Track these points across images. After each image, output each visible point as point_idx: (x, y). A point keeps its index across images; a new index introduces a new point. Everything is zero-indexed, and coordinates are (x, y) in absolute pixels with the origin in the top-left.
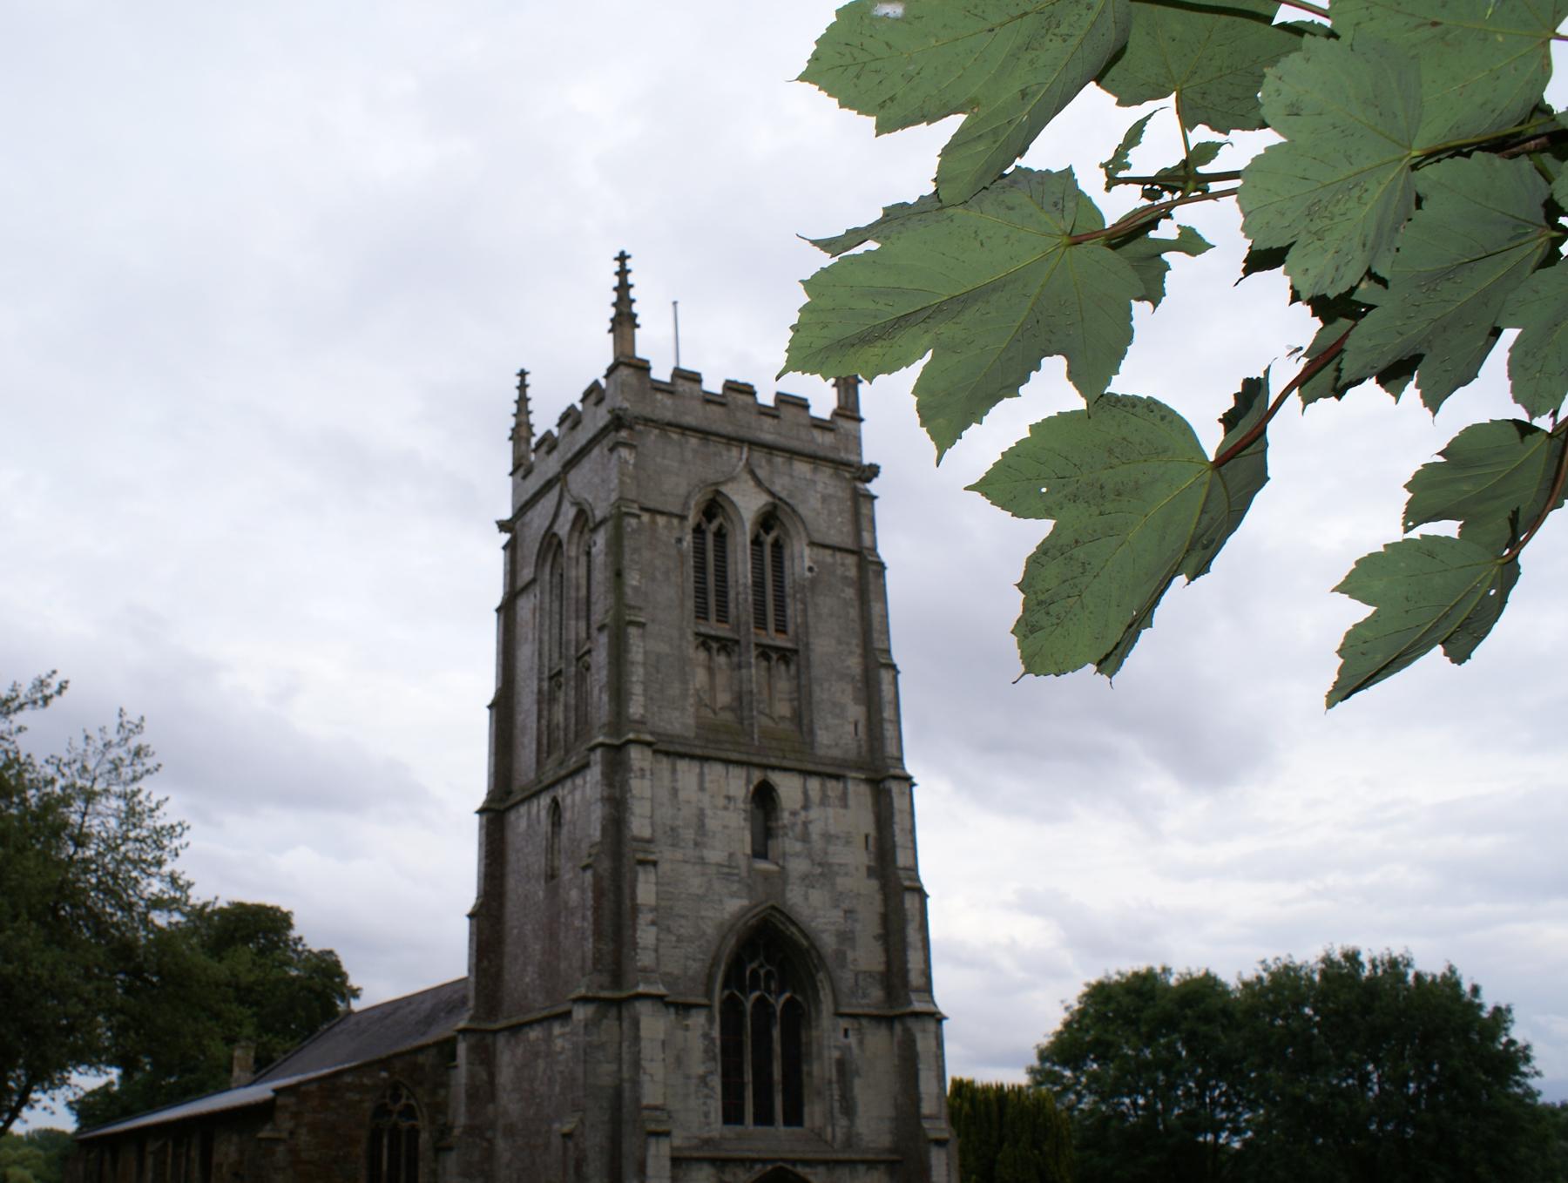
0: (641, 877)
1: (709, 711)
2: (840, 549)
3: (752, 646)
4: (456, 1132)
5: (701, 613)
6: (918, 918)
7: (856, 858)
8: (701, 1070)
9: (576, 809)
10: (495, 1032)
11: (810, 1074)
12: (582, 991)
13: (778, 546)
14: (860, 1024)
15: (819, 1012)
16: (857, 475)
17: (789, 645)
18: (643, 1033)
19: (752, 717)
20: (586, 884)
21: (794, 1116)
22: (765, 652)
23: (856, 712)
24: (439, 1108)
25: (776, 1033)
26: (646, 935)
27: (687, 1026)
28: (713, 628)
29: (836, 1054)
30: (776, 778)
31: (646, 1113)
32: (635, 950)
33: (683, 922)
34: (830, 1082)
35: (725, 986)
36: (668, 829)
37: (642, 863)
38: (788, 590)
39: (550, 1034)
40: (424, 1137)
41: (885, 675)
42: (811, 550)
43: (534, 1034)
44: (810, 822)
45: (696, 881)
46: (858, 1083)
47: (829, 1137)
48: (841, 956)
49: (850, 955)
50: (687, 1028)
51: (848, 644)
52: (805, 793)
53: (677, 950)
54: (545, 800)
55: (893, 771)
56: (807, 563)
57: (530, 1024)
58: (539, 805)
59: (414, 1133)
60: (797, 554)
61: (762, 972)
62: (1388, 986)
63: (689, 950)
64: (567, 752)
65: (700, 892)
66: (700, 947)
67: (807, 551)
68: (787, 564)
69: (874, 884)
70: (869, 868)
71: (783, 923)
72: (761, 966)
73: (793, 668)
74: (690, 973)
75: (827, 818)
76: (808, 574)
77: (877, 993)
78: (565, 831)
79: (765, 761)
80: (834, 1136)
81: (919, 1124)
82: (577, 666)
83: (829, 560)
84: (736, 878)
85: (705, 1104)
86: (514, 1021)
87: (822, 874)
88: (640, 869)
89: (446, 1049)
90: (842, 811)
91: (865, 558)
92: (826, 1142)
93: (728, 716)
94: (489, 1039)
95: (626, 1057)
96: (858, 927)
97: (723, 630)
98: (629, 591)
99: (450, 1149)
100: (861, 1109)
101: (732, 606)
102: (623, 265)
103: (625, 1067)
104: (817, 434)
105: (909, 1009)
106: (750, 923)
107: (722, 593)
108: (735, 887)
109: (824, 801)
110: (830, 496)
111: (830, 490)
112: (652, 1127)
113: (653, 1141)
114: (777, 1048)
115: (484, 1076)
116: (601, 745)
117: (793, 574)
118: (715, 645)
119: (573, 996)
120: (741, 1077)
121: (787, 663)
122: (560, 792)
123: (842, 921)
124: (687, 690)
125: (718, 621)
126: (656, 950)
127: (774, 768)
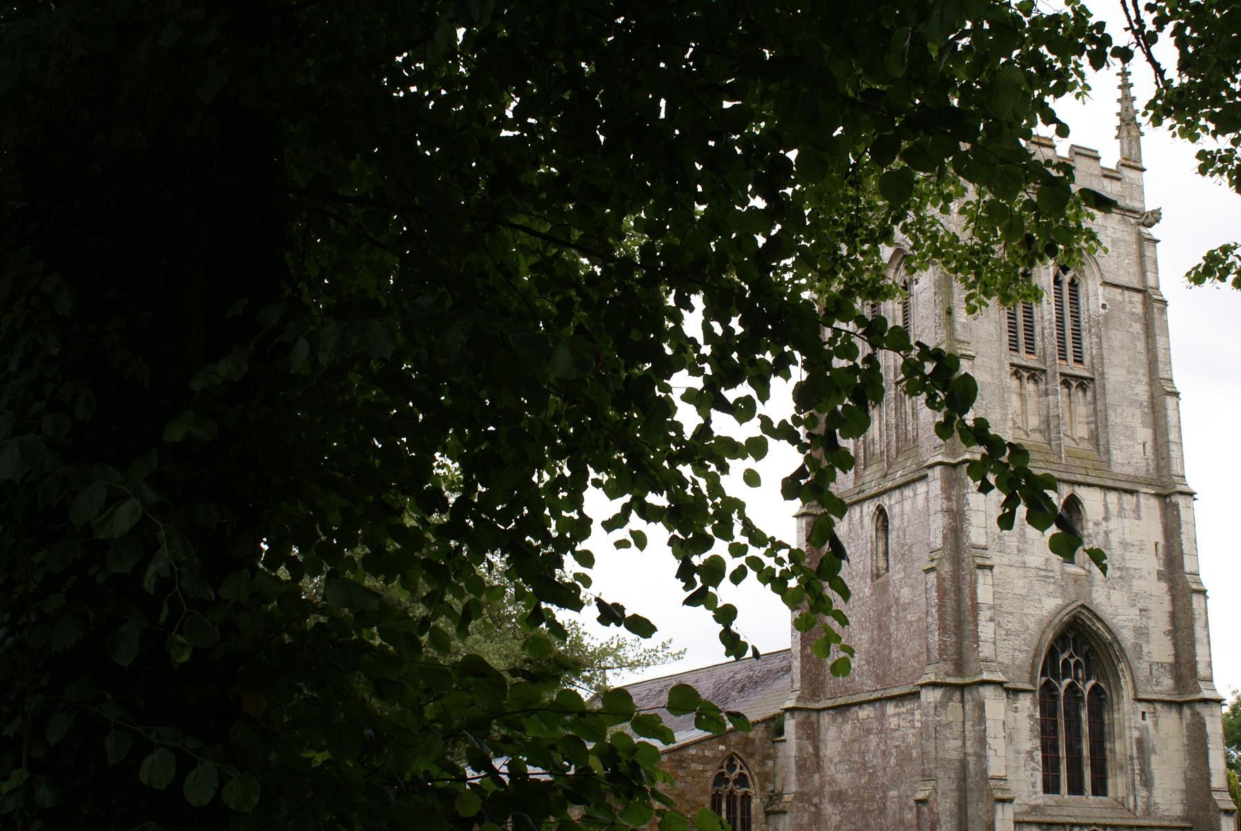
0: (981, 579)
1: (1022, 432)
2: (1128, 288)
3: (1058, 375)
4: (787, 798)
5: (1014, 347)
6: (1203, 617)
7: (1149, 563)
8: (1028, 746)
9: (906, 517)
10: (819, 711)
11: (1113, 751)
12: (932, 678)
13: (1073, 284)
14: (1155, 708)
15: (1120, 697)
16: (1141, 221)
17: (1086, 374)
18: (988, 714)
19: (1060, 439)
20: (929, 585)
21: (1100, 788)
22: (1067, 380)
23: (1145, 434)
24: (767, 777)
25: (1084, 715)
26: (986, 630)
27: (1016, 708)
28: (1023, 359)
29: (1136, 734)
30: (1081, 492)
31: (992, 783)
32: (977, 643)
33: (1010, 618)
34: (1131, 758)
35: (1042, 675)
36: (996, 537)
37: (981, 567)
38: (1084, 324)
39: (883, 714)
40: (756, 803)
41: (1170, 401)
42: (1104, 289)
43: (864, 713)
44: (1110, 531)
45: (1021, 583)
46: (1154, 760)
47: (1131, 806)
48: (1138, 648)
49: (1145, 649)
50: (1016, 710)
51: (1136, 373)
52: (1106, 506)
53: (1006, 642)
54: (869, 508)
55: (1179, 488)
56: (1101, 302)
57: (860, 704)
58: (862, 511)
59: (747, 798)
60: (1091, 293)
61: (1072, 661)
62: (319, 598)
63: (1016, 642)
64: (889, 467)
65: (1023, 592)
66: (1024, 640)
67: (1101, 289)
68: (1082, 301)
69: (1163, 586)
70: (1159, 572)
71: (1090, 619)
72: (1071, 656)
73: (1089, 394)
74: (1018, 661)
75: (1124, 528)
76: (1102, 311)
77: (1167, 682)
78: (892, 536)
79: (1073, 478)
80: (1135, 806)
81: (1210, 795)
82: (896, 389)
83: (1119, 298)
84: (882, 564)
85: (1032, 775)
86: (840, 701)
87: (1120, 577)
88: (979, 572)
89: (775, 726)
90: (1137, 522)
91: (1150, 296)
92: (1129, 810)
93: (1037, 437)
94: (814, 717)
95: (970, 734)
96: (1151, 624)
97: (1031, 362)
98: (958, 327)
99: (784, 812)
100: (1157, 782)
101: (1038, 339)
102: (1125, 80)
103: (969, 743)
104: (1106, 182)
105: (1200, 696)
106: (1064, 620)
107: (1030, 328)
108: (1051, 588)
109: (1121, 512)
110: (1119, 240)
111: (1119, 235)
112: (999, 795)
113: (999, 806)
114: (1085, 728)
115: (811, 750)
116: (940, 463)
117: (1088, 310)
118: (1026, 375)
119: (920, 682)
120: (1057, 752)
121: (1084, 390)
122: (886, 501)
123: (1138, 618)
124: (1006, 415)
125: (1075, 361)
126: (994, 643)
127: (1079, 484)
